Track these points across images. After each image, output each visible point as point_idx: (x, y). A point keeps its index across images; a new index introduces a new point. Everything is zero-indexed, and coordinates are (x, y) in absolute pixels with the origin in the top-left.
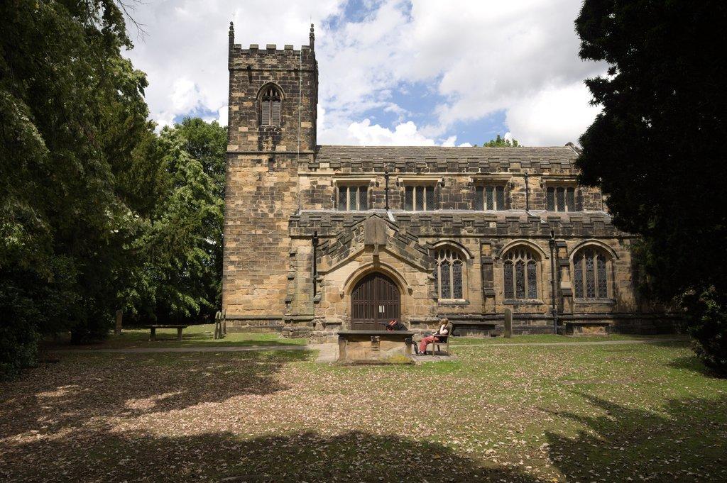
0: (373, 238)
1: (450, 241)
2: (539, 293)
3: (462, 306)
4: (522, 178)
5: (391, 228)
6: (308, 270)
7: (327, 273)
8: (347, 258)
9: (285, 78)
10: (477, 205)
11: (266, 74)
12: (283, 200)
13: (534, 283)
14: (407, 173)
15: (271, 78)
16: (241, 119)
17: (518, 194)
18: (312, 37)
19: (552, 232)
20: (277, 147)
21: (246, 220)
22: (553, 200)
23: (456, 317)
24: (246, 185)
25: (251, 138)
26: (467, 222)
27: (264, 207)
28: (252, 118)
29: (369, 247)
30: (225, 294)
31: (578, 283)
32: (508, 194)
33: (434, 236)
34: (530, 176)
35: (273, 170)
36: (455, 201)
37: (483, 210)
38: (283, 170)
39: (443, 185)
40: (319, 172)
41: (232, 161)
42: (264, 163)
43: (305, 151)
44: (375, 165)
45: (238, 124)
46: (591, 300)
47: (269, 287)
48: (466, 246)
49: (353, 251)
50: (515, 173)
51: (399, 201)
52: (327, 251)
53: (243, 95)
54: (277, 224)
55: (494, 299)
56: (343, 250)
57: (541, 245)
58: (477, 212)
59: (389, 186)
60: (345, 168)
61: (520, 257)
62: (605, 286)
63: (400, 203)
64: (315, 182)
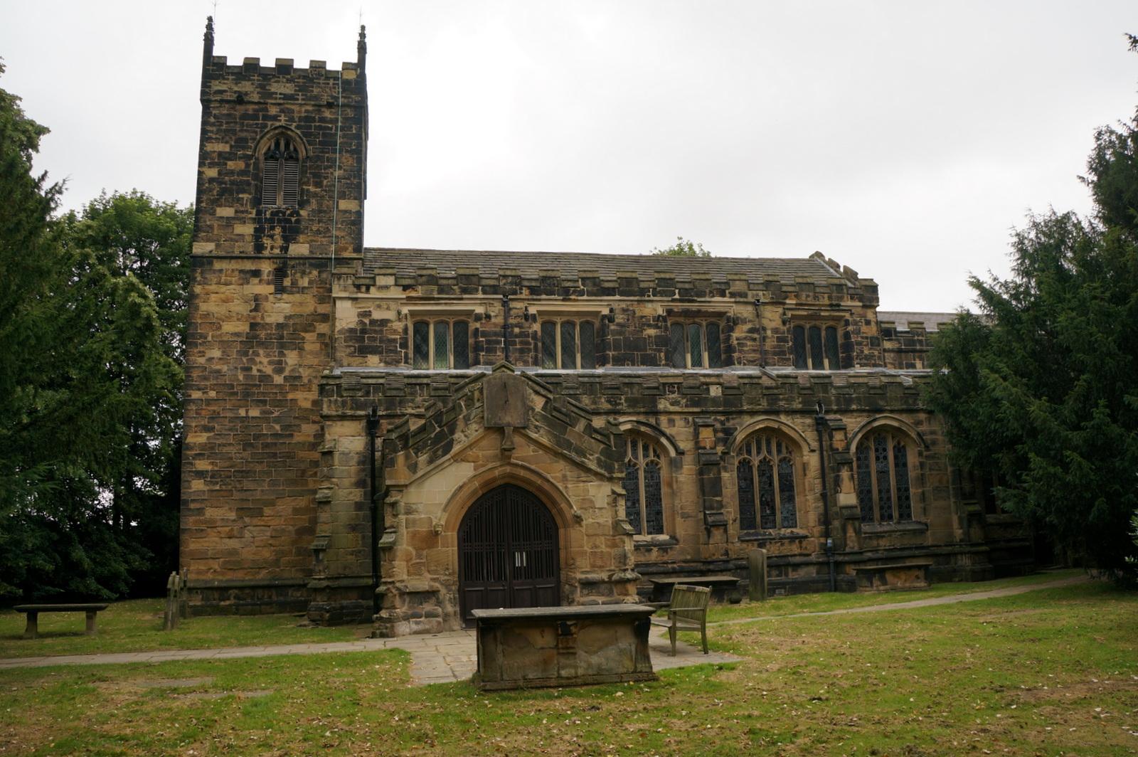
1: (638, 422)
3: (663, 547)
4: (750, 308)
5: (537, 393)
6: (360, 484)
9: (308, 119)
12: (301, 349)
13: (791, 499)
14: (544, 297)
15: (283, 118)
16: (222, 192)
17: (745, 338)
18: (362, 48)
21: (228, 389)
24: (228, 318)
25: (239, 229)
26: (664, 388)
27: (263, 362)
28: (244, 192)
30: (184, 537)
32: (729, 338)
33: (608, 413)
36: (633, 351)
37: (685, 367)
41: (202, 273)
42: (265, 277)
43: (346, 255)
44: (484, 282)
45: (216, 202)
46: (886, 527)
48: (668, 431)
50: (738, 299)
51: (529, 350)
53: (227, 149)
54: (290, 396)
56: (440, 437)
57: (799, 427)
60: (425, 287)
61: (764, 452)
62: (908, 498)
64: (368, 314)
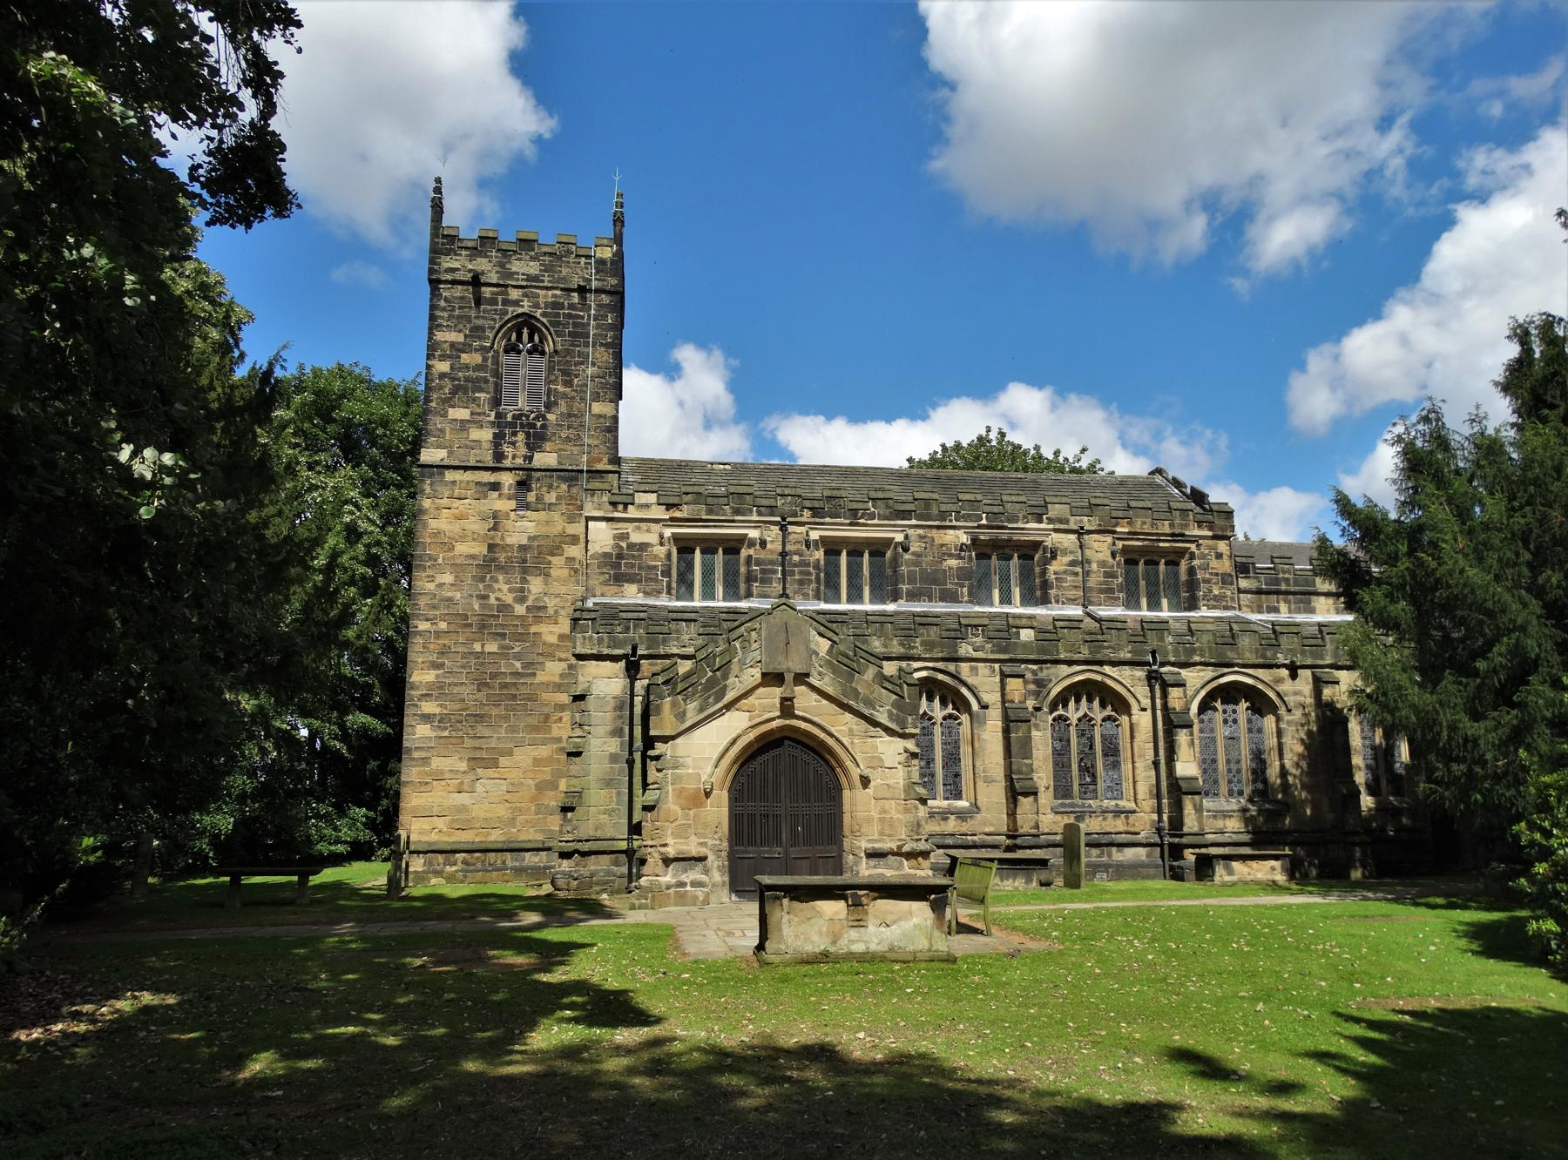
0: (781, 658)
1: (934, 669)
2: (1127, 787)
3: (962, 815)
4: (1073, 537)
5: (821, 634)
6: (617, 732)
7: (673, 738)
8: (720, 705)
9: (556, 305)
10: (979, 592)
11: (514, 294)
12: (547, 575)
13: (1116, 765)
14: (828, 520)
15: (526, 303)
16: (454, 392)
18: (619, 220)
19: (1153, 653)
20: (537, 456)
21: (462, 621)
22: (1137, 585)
23: (950, 841)
24: (462, 538)
25: (475, 434)
27: (503, 590)
28: (481, 390)
29: (773, 678)
31: (1208, 764)
32: (1044, 572)
34: (1089, 532)
35: (527, 507)
36: (931, 584)
38: (550, 507)
39: (906, 550)
40: (632, 512)
43: (600, 467)
45: (448, 402)
47: (514, 775)
48: (970, 681)
49: (735, 687)
51: (810, 581)
52: (674, 688)
53: (460, 338)
54: (533, 629)
55: (1036, 800)
56: (712, 683)
57: (1129, 681)
58: (977, 609)
59: (789, 548)
63: (814, 585)
